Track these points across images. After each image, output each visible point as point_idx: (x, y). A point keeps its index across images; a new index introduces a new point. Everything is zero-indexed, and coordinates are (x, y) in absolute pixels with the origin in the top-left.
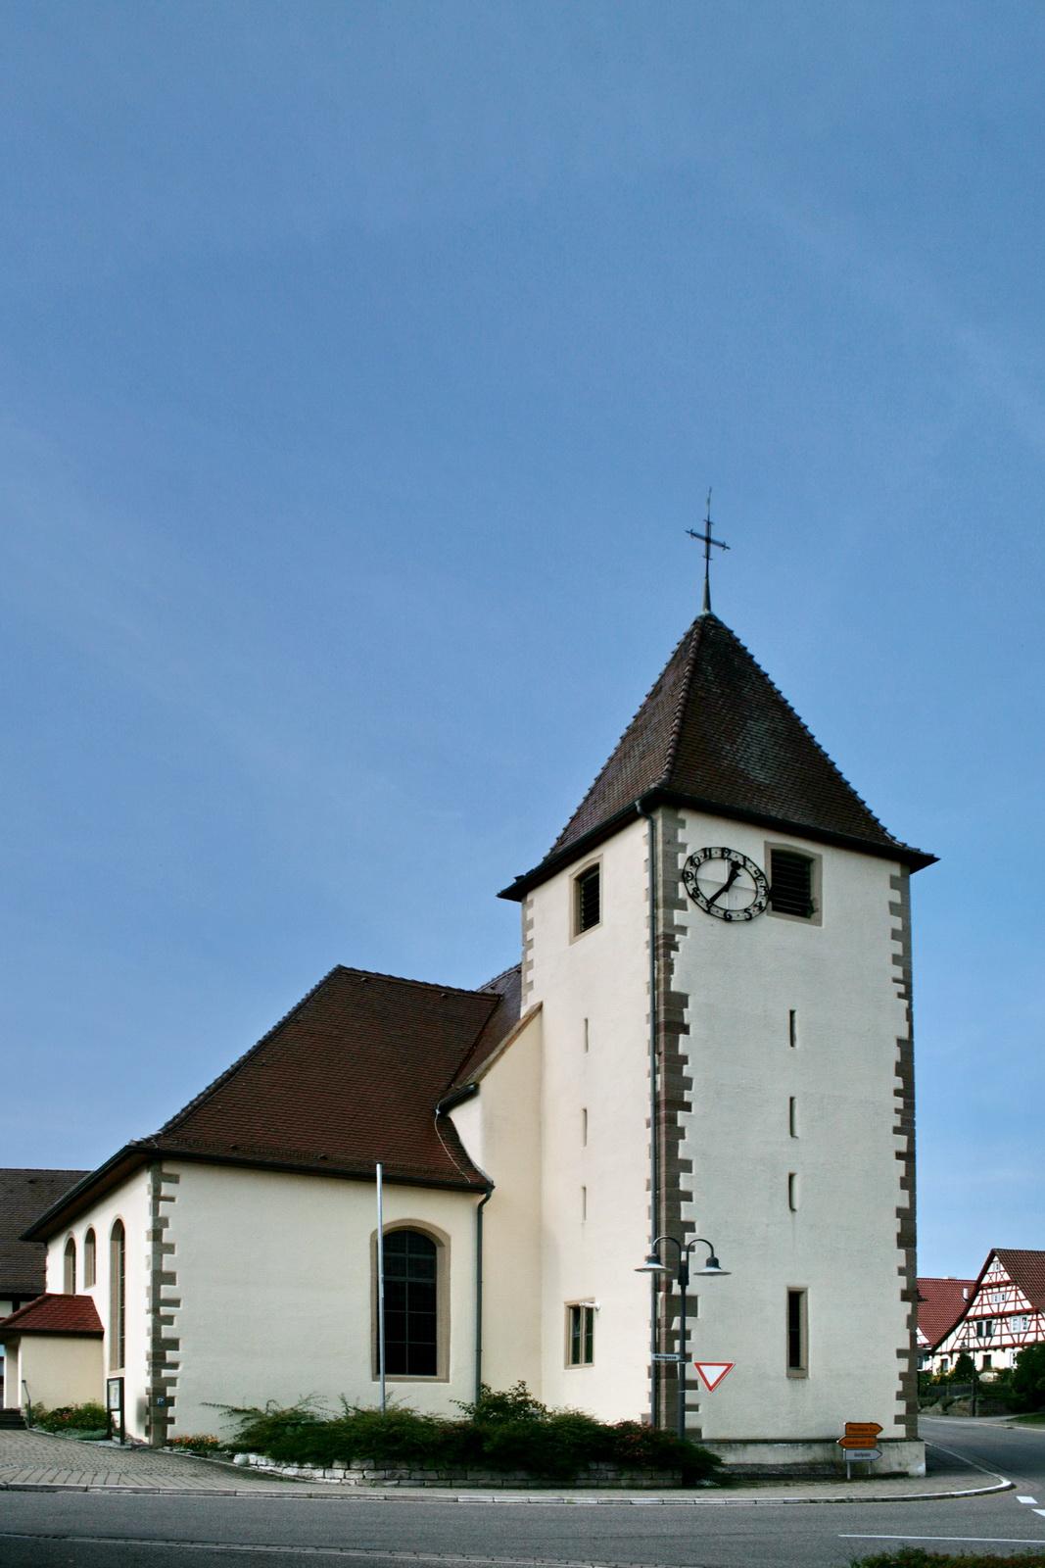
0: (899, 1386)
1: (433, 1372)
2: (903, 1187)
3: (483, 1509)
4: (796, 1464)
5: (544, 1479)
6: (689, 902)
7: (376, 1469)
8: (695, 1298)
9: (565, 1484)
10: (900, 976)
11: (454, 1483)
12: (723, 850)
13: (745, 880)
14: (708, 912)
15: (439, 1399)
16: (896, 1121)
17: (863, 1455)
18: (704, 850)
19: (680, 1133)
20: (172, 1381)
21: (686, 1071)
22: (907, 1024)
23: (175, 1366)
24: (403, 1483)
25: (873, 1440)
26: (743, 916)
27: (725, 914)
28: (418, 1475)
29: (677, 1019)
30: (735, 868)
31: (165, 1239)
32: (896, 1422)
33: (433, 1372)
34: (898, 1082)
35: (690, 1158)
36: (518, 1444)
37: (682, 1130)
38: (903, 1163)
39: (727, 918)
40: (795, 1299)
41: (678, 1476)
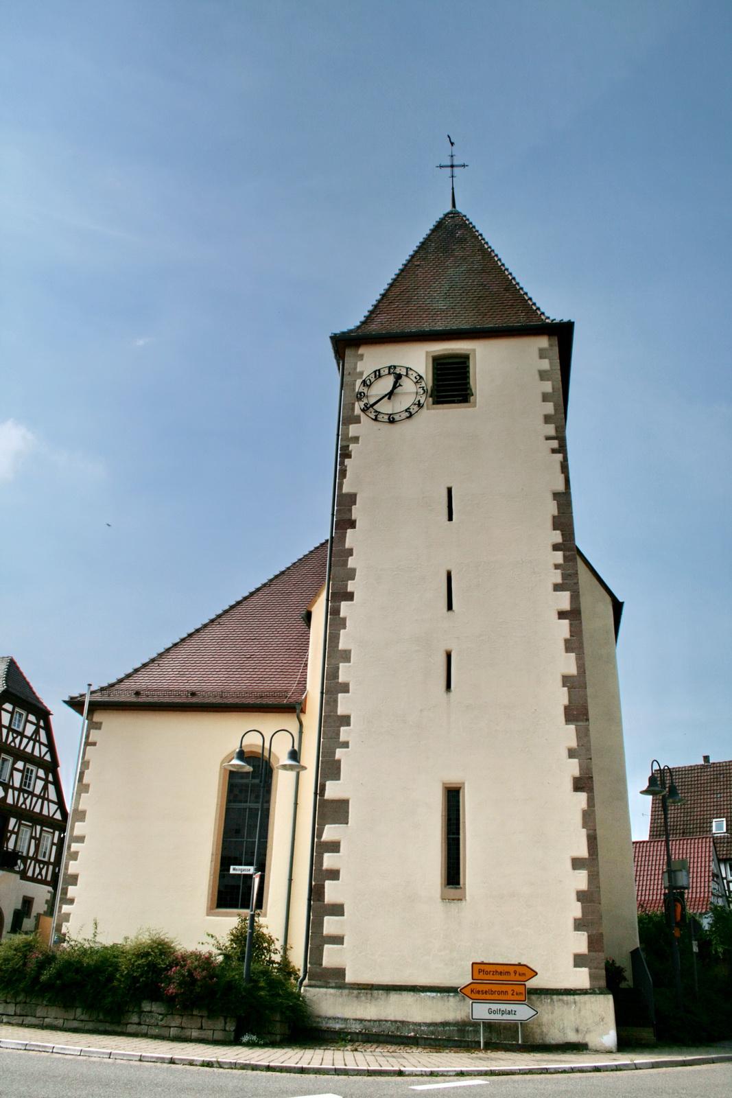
0: (576, 910)
2: (568, 649)
3: (541, 1083)
4: (445, 1024)
5: (101, 1021)
6: (362, 415)
10: (552, 432)
11: (29, 1020)
12: (390, 368)
13: (408, 385)
14: (376, 420)
17: (503, 1013)
18: (375, 372)
19: (342, 623)
22: (562, 476)
25: (521, 989)
27: (389, 419)
29: (346, 517)
32: (576, 965)
34: (557, 537)
37: (344, 619)
38: (566, 622)
39: (392, 421)
40: (453, 797)
41: (231, 1027)
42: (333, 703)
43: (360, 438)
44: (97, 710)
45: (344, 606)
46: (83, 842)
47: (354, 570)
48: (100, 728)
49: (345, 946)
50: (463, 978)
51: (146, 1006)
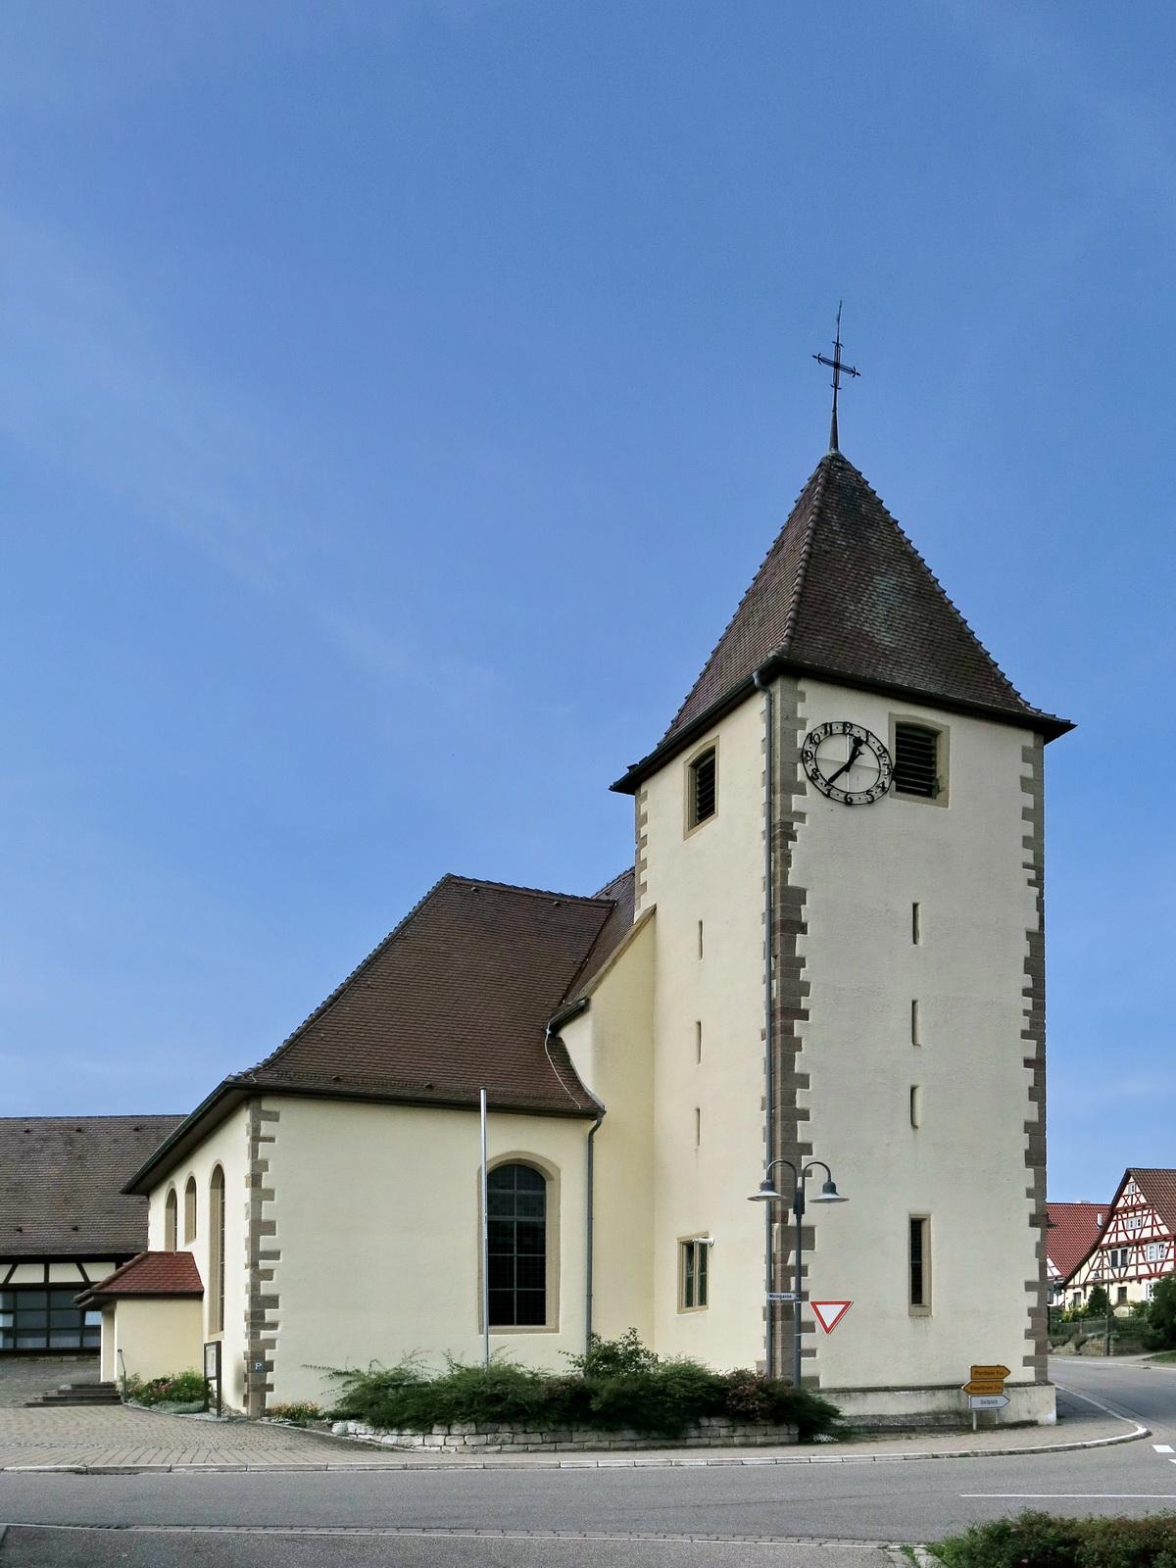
1: (543, 1322)
2: (1032, 1098)
4: (919, 1414)
5: (654, 1439)
6: (808, 784)
7: (478, 1434)
8: (812, 1229)
9: (674, 1443)
10: (1031, 861)
11: (559, 1446)
12: (845, 724)
13: (867, 758)
14: (828, 796)
15: (546, 1353)
16: (1025, 1023)
17: (989, 1402)
18: (825, 725)
19: (797, 1045)
20: (271, 1343)
21: (804, 974)
23: (274, 1326)
24: (506, 1448)
26: (865, 798)
28: (521, 1438)
29: (796, 918)
30: (858, 742)
31: (264, 1184)
33: (543, 1322)
34: (1027, 981)
35: (807, 1072)
36: (636, 1403)
37: (799, 1040)
38: (1032, 1071)
39: (848, 802)
40: (917, 1226)
41: (795, 1431)
42: (791, 1131)
43: (807, 817)
44: (267, 1095)
45: (798, 1026)
46: (278, 1259)
47: (808, 985)
48: (277, 1120)
49: (817, 1358)
50: (965, 1377)
51: (704, 1422)
